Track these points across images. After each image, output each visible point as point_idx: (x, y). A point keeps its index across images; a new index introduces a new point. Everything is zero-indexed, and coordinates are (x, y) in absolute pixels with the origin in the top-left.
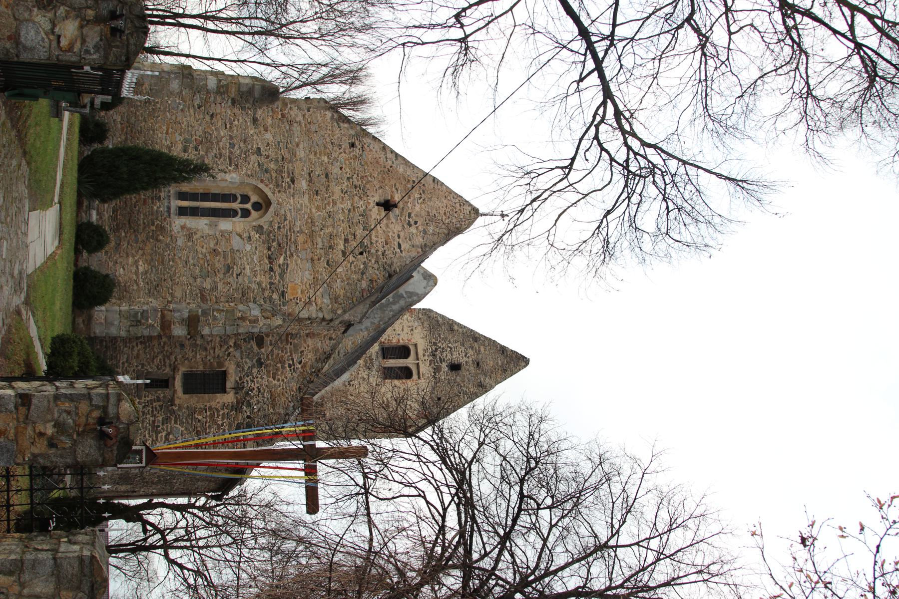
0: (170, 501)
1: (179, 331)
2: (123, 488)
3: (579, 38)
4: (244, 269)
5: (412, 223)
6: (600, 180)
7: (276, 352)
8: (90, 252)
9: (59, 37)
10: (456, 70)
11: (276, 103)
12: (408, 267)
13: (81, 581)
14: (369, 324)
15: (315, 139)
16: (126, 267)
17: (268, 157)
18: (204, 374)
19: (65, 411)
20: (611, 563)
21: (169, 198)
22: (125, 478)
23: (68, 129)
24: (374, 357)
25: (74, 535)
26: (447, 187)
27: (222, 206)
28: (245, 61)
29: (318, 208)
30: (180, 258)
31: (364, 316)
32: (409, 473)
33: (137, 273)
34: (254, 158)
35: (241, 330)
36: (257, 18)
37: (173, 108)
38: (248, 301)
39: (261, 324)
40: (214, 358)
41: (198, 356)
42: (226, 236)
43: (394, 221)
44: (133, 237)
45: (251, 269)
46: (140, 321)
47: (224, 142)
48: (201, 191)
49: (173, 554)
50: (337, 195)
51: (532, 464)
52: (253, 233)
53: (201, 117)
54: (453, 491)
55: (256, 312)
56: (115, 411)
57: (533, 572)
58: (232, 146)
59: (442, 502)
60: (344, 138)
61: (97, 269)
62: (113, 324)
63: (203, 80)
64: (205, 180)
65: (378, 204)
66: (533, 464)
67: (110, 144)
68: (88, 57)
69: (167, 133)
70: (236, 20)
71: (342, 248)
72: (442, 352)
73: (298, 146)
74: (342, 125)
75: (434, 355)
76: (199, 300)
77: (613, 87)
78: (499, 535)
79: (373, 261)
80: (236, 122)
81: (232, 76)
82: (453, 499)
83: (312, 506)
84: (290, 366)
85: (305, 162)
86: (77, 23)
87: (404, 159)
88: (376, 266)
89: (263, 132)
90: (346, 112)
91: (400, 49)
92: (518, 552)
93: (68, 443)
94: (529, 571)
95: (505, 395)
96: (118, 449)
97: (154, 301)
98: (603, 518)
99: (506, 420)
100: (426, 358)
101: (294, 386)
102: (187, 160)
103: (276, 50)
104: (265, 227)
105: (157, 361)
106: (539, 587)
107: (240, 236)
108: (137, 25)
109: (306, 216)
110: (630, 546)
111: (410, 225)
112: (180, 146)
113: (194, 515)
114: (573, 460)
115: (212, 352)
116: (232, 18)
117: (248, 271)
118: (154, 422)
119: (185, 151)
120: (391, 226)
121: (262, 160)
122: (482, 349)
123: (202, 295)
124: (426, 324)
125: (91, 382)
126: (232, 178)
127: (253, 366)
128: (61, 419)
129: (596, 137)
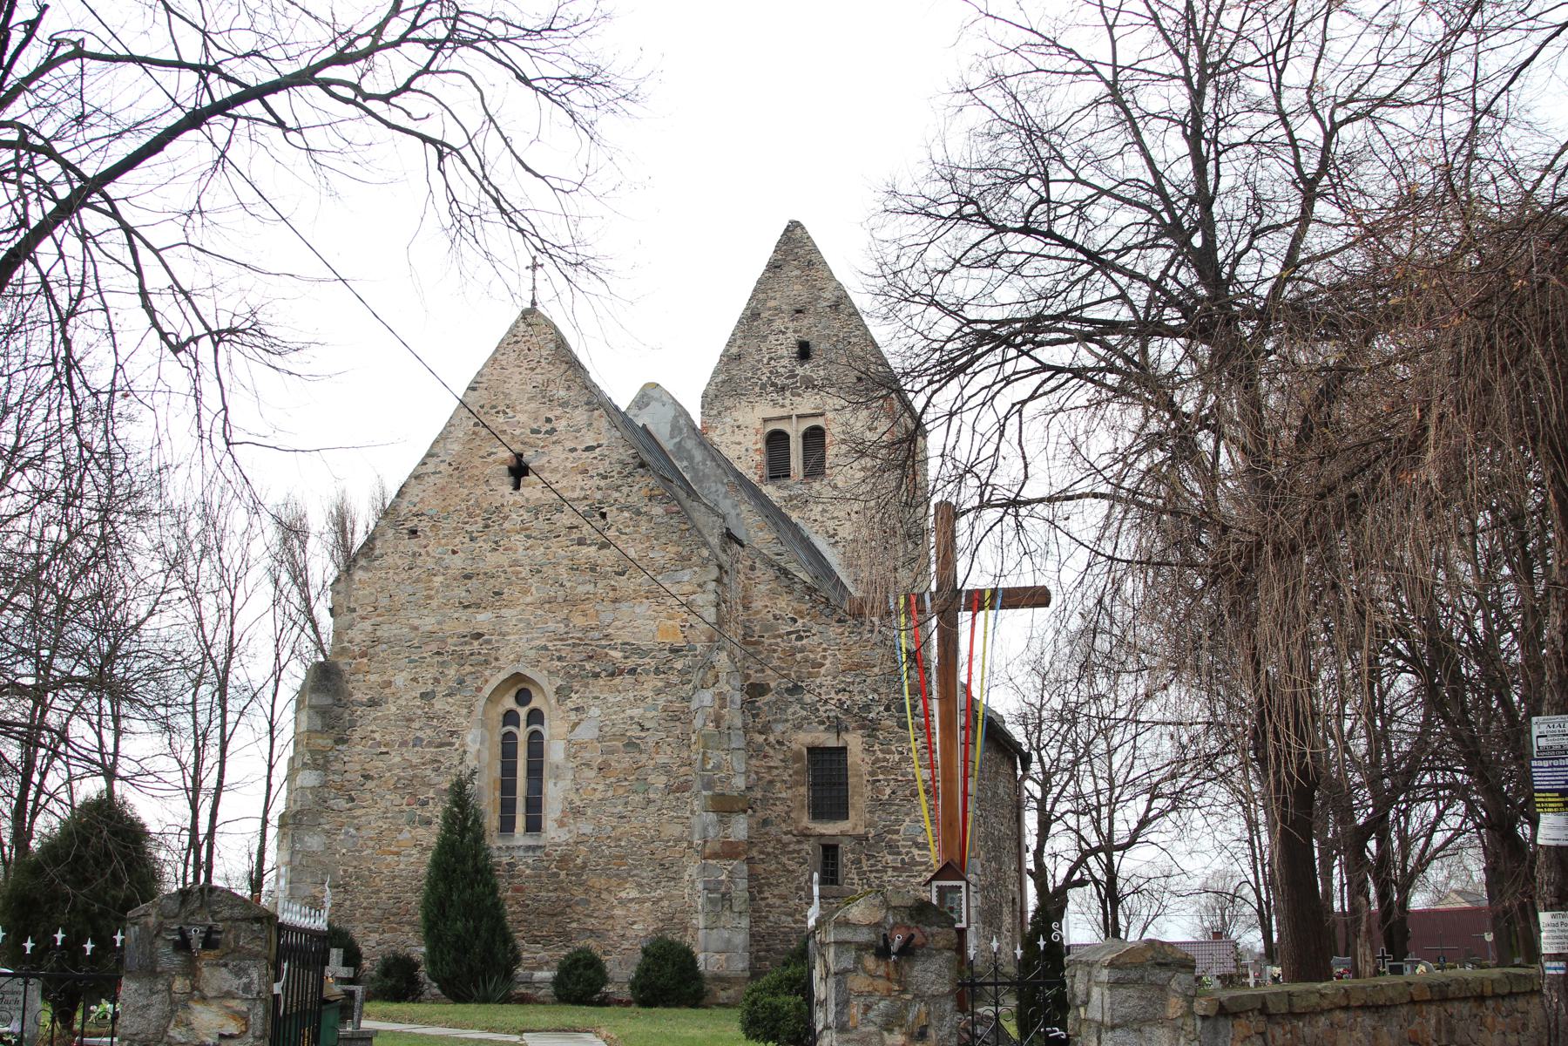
0: (1031, 841)
1: (740, 828)
2: (1007, 920)
3: (205, 127)
4: (632, 718)
5: (548, 427)
6: (461, 93)
7: (775, 663)
8: (605, 980)
9: (222, 1036)
10: (276, 349)
11: (342, 666)
12: (627, 434)
13: (1152, 984)
14: (728, 502)
15: (403, 597)
16: (630, 920)
17: (436, 680)
18: (814, 786)
19: (865, 1013)
20: (1144, 76)
21: (509, 849)
22: (990, 917)
23: (394, 1021)
24: (786, 493)
25: (1075, 996)
26: (485, 365)
27: (521, 759)
28: (271, 723)
29: (525, 592)
30: (614, 828)
31: (712, 510)
32: (980, 428)
33: (641, 901)
34: (439, 704)
35: (738, 722)
36: (194, 703)
37: (355, 844)
38: (687, 712)
39: (727, 687)
40: (786, 768)
41: (784, 795)
42: (574, 749)
43: (545, 459)
44: (579, 908)
45: (632, 706)
46: (723, 895)
47: (413, 756)
48: (498, 794)
49: (1122, 832)
50: (501, 558)
51: (971, 210)
52: (570, 704)
53: (368, 796)
54: (1012, 352)
55: (706, 697)
56: (865, 930)
57: (1157, 214)
58: (418, 742)
59: (1033, 372)
60: (401, 548)
61: (634, 968)
62: (729, 940)
63: (303, 795)
64: (480, 788)
65: (517, 487)
66: (969, 209)
67: (419, 951)
68: (255, 988)
69: (398, 854)
70: (200, 739)
71: (594, 548)
72: (778, 374)
73: (416, 628)
74: (377, 552)
75: (783, 389)
76: (687, 794)
77: (288, 69)
78: (1091, 273)
79: (617, 495)
80: (377, 736)
81: (296, 744)
82: (1027, 354)
83: (1037, 597)
84: (800, 638)
85: (444, 615)
86: (198, 1007)
87: (436, 442)
88: (625, 490)
89: (393, 689)
90: (359, 539)
91: (236, 449)
92: (1125, 237)
93: (918, 1009)
94: (1155, 221)
95: (849, 262)
96: (930, 925)
97: (689, 871)
98: (1063, 89)
99: (891, 259)
100: (787, 402)
101: (834, 630)
102: (445, 819)
103: (252, 669)
104: (559, 682)
105: (792, 865)
106: (1183, 203)
107: (576, 725)
108: (197, 904)
109: (540, 612)
110: (1114, 42)
111: (553, 430)
112: (421, 831)
113: (1056, 800)
114: (964, 138)
115: (775, 772)
116: (196, 747)
117: (636, 712)
118: (895, 869)
119: (429, 822)
120: (555, 463)
121: (441, 689)
122: (772, 304)
123: (678, 790)
124: (728, 403)
125: (817, 974)
126: (474, 741)
127: (800, 701)
128: (878, 1020)
129: (386, 98)
